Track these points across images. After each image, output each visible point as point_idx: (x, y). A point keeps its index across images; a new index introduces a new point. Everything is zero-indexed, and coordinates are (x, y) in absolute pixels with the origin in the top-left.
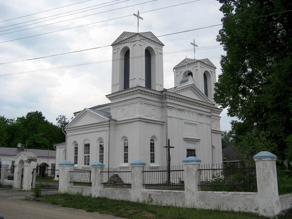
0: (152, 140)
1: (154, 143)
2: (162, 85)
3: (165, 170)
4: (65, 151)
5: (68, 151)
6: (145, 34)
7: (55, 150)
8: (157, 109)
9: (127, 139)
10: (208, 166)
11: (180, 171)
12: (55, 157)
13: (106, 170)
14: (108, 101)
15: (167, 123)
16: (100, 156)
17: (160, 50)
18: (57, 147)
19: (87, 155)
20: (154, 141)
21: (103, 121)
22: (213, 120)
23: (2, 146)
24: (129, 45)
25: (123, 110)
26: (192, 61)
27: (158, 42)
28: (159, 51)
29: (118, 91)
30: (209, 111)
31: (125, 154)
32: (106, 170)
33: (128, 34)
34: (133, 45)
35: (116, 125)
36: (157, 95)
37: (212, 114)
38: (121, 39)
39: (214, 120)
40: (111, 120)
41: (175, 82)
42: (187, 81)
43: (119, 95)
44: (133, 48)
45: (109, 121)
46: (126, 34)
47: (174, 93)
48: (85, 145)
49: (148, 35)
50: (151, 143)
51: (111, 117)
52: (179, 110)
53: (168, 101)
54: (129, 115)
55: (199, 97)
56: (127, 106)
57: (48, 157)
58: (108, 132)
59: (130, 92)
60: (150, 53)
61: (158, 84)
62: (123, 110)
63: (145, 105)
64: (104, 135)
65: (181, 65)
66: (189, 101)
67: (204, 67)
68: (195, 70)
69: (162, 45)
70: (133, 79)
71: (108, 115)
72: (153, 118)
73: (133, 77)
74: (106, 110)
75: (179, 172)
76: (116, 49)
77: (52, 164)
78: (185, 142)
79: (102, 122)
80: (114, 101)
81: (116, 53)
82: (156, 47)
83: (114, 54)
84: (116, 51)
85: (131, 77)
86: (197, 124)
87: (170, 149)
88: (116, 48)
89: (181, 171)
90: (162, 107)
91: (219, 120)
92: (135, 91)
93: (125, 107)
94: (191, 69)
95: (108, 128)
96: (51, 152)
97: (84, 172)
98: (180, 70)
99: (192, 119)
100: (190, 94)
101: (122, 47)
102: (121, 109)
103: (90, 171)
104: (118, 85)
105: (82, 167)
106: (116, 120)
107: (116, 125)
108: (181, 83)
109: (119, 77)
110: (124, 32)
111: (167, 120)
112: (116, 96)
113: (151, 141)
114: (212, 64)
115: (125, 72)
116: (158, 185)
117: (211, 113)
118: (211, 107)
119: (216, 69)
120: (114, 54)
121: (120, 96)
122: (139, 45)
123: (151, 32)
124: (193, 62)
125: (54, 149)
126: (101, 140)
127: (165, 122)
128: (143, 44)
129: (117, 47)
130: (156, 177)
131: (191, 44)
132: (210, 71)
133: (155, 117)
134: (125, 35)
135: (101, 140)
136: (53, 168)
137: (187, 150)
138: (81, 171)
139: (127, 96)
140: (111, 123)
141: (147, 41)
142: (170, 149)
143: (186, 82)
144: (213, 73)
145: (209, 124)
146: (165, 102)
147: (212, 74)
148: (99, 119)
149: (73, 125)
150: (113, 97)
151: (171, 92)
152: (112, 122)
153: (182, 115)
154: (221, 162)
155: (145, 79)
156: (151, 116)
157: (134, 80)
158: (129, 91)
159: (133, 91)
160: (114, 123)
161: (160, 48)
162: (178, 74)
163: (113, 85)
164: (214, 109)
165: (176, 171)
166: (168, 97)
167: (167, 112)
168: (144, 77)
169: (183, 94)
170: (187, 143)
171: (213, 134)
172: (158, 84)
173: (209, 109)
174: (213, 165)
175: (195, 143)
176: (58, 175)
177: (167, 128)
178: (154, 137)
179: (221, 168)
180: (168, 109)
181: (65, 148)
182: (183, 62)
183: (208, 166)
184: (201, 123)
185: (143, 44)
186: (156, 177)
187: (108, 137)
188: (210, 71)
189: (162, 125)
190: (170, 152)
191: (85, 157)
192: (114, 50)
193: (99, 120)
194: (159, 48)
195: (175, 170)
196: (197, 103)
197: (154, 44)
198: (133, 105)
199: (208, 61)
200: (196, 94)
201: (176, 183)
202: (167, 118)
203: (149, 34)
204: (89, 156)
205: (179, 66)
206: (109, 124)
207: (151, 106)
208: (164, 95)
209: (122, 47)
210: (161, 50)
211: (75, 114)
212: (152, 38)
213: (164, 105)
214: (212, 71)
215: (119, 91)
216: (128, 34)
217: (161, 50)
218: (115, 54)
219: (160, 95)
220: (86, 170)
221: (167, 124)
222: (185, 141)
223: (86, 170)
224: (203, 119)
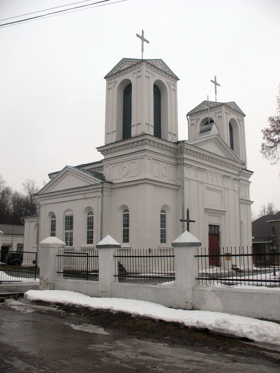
0: (162, 210)
1: (165, 215)
2: (176, 135)
3: (90, 258)
4: (38, 226)
5: (42, 226)
7: (23, 225)
8: (170, 167)
9: (127, 210)
10: (142, 251)
11: (141, 257)
12: (23, 235)
13: (31, 255)
14: (100, 157)
15: (184, 187)
16: (88, 234)
17: (173, 86)
18: (25, 220)
19: (69, 231)
20: (165, 212)
21: (93, 184)
22: (242, 185)
24: (130, 76)
25: (121, 169)
26: (213, 104)
27: (170, 74)
28: (172, 87)
29: (115, 141)
30: (237, 173)
31: (124, 230)
32: (31, 255)
33: (129, 61)
34: (137, 77)
35: (112, 189)
36: (170, 147)
37: (241, 177)
38: (119, 68)
39: (243, 186)
40: (105, 182)
41: (189, 134)
42: (210, 129)
43: (115, 147)
44: (137, 81)
45: (102, 183)
46: (126, 61)
47: (193, 146)
48: (66, 217)
49: (158, 63)
50: (161, 215)
51: (104, 179)
54: (131, 175)
56: (128, 162)
57: (13, 235)
58: (100, 200)
59: (133, 143)
60: (160, 90)
61: (171, 133)
62: (121, 169)
63: (155, 161)
64: (95, 205)
65: (198, 110)
67: (229, 113)
69: (176, 78)
70: (137, 124)
71: (101, 176)
72: (164, 180)
73: (137, 121)
74: (97, 169)
75: (134, 258)
76: (112, 83)
77: (18, 244)
79: (91, 185)
80: (109, 156)
81: (111, 88)
83: (108, 89)
84: (111, 86)
85: (133, 122)
87: (190, 223)
88: (112, 81)
89: (139, 258)
90: (177, 165)
92: (135, 142)
93: (125, 164)
94: (211, 115)
95: (99, 194)
96: (17, 228)
97: (68, 256)
98: (196, 117)
100: (212, 148)
101: (120, 79)
102: (119, 167)
103: (87, 254)
104: (115, 133)
105: (83, 249)
106: (111, 183)
107: (112, 189)
108: (200, 133)
109: (117, 122)
110: (124, 59)
111: (183, 182)
112: (111, 149)
113: (161, 212)
114: (167, 67)
115: (124, 115)
116: (154, 277)
117: (239, 175)
119: (178, 81)
120: (108, 89)
121: (131, 145)
122: (146, 76)
123: (161, 60)
124: (215, 105)
125: (22, 224)
126: (90, 211)
127: (180, 186)
128: (150, 76)
129: (114, 80)
130: (148, 264)
131: (212, 81)
132: (238, 119)
134: (124, 62)
135: (90, 211)
136: (19, 249)
137: (210, 225)
138: (80, 255)
139: (127, 148)
140: (104, 186)
141: (155, 72)
142: (190, 223)
143: (208, 132)
144: (241, 122)
146: (180, 157)
147: (239, 122)
148: (87, 181)
149: (50, 189)
150: (107, 150)
151: (46, 192)
152: (106, 185)
153: (202, 177)
154: (250, 244)
155: (153, 124)
156: (161, 176)
157: (139, 126)
158: (131, 141)
159: (138, 142)
160: (110, 187)
161: (174, 84)
162: (193, 122)
163: (107, 134)
165: (136, 257)
167: (183, 172)
168: (152, 123)
169: (205, 147)
171: (241, 205)
172: (171, 133)
174: (240, 248)
176: (35, 260)
177: (183, 194)
178: (165, 206)
179: (250, 253)
181: (37, 222)
182: (203, 104)
183: (142, 251)
186: (148, 264)
187: (100, 206)
188: (238, 119)
189: (177, 190)
190: (189, 227)
191: (67, 234)
192: (108, 84)
193: (85, 181)
194: (172, 83)
195: (160, 258)
197: (166, 77)
198: (136, 161)
199: (235, 105)
200: (220, 148)
201: (84, 270)
203: (159, 62)
204: (72, 234)
206: (102, 188)
207: (161, 163)
208: (180, 147)
209: (120, 79)
210: (175, 85)
211: (50, 175)
213: (179, 162)
214: (240, 120)
215: (116, 142)
216: (129, 61)
218: (110, 90)
219: (174, 149)
220: (83, 254)
221: (183, 189)
223: (83, 254)
224: (228, 184)
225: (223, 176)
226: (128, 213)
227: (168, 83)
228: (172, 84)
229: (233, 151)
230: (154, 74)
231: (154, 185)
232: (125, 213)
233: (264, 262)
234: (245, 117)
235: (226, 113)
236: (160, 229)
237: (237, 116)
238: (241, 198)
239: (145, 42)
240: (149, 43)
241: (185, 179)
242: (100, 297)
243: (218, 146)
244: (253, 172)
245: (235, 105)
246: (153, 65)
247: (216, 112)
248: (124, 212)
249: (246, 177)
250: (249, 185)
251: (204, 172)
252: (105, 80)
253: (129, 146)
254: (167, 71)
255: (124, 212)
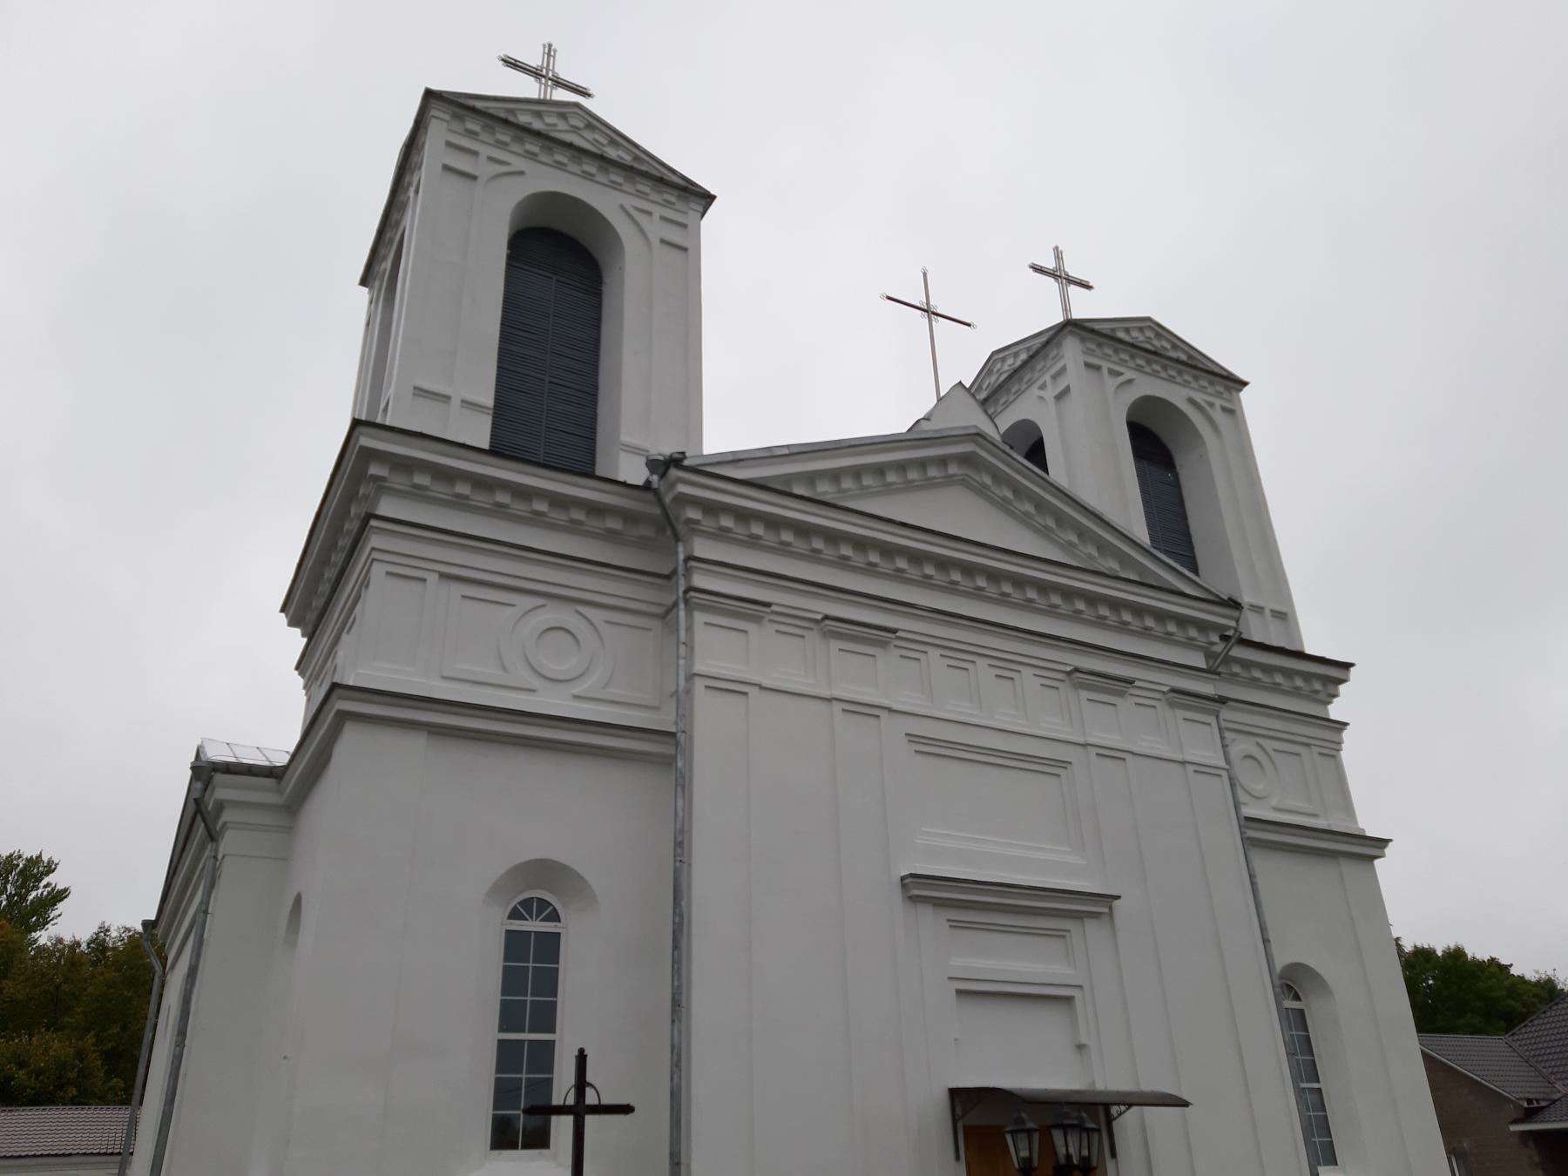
6: (1127, 330)
22: (595, 615)
23: (1547, 991)
26: (1016, 355)
27: (1184, 357)
30: (1199, 660)
52: (832, 627)
53: (703, 548)
55: (1045, 533)
63: (458, 589)
66: (943, 564)
68: (1051, 401)
78: (929, 918)
82: (629, 202)
86: (1064, 764)
90: (666, 615)
91: (1332, 751)
99: (1006, 717)
118: (1203, 626)
119: (1245, 395)
124: (1024, 356)
132: (1191, 401)
133: (576, 697)
145: (1203, 769)
156: (535, 683)
161: (675, 235)
164: (1239, 652)
166: (693, 514)
170: (956, 925)
172: (1258, 609)
173: (1190, 644)
175: (1060, 935)
180: (700, 618)
184: (1110, 754)
185: (483, 169)
188: (1191, 401)
194: (1218, 402)
196: (1044, 588)
197: (614, 186)
200: (1003, 506)
202: (689, 691)
205: (512, 111)
212: (575, 129)
214: (1211, 405)
217: (685, 249)
222: (927, 914)
225: (1069, 673)
226: (548, 927)
227: (634, 213)
228: (663, 218)
229: (1196, 572)
230: (518, 163)
231: (431, 733)
232: (518, 925)
233: (557, 1100)
234: (1242, 394)
235: (1098, 368)
236: (491, 1035)
237: (1186, 384)
238: (1249, 811)
239: (1073, 289)
240: (1088, 287)
241: (699, 684)
242: (1308, 1039)
243: (981, 491)
244: (1347, 666)
245: (1158, 335)
246: (1153, 349)
247: (1040, 382)
248: (515, 915)
249: (1313, 697)
250: (1339, 743)
251: (1121, 694)
252: (367, 289)
253: (594, 524)
254: (1168, 346)
255: (515, 915)
